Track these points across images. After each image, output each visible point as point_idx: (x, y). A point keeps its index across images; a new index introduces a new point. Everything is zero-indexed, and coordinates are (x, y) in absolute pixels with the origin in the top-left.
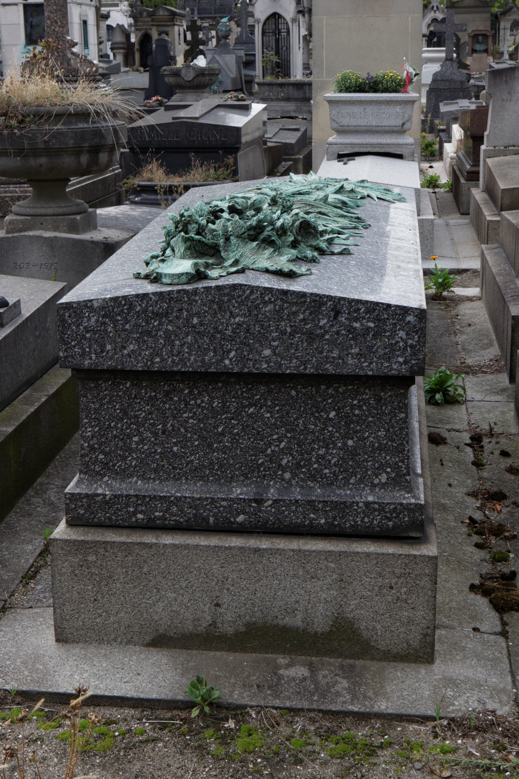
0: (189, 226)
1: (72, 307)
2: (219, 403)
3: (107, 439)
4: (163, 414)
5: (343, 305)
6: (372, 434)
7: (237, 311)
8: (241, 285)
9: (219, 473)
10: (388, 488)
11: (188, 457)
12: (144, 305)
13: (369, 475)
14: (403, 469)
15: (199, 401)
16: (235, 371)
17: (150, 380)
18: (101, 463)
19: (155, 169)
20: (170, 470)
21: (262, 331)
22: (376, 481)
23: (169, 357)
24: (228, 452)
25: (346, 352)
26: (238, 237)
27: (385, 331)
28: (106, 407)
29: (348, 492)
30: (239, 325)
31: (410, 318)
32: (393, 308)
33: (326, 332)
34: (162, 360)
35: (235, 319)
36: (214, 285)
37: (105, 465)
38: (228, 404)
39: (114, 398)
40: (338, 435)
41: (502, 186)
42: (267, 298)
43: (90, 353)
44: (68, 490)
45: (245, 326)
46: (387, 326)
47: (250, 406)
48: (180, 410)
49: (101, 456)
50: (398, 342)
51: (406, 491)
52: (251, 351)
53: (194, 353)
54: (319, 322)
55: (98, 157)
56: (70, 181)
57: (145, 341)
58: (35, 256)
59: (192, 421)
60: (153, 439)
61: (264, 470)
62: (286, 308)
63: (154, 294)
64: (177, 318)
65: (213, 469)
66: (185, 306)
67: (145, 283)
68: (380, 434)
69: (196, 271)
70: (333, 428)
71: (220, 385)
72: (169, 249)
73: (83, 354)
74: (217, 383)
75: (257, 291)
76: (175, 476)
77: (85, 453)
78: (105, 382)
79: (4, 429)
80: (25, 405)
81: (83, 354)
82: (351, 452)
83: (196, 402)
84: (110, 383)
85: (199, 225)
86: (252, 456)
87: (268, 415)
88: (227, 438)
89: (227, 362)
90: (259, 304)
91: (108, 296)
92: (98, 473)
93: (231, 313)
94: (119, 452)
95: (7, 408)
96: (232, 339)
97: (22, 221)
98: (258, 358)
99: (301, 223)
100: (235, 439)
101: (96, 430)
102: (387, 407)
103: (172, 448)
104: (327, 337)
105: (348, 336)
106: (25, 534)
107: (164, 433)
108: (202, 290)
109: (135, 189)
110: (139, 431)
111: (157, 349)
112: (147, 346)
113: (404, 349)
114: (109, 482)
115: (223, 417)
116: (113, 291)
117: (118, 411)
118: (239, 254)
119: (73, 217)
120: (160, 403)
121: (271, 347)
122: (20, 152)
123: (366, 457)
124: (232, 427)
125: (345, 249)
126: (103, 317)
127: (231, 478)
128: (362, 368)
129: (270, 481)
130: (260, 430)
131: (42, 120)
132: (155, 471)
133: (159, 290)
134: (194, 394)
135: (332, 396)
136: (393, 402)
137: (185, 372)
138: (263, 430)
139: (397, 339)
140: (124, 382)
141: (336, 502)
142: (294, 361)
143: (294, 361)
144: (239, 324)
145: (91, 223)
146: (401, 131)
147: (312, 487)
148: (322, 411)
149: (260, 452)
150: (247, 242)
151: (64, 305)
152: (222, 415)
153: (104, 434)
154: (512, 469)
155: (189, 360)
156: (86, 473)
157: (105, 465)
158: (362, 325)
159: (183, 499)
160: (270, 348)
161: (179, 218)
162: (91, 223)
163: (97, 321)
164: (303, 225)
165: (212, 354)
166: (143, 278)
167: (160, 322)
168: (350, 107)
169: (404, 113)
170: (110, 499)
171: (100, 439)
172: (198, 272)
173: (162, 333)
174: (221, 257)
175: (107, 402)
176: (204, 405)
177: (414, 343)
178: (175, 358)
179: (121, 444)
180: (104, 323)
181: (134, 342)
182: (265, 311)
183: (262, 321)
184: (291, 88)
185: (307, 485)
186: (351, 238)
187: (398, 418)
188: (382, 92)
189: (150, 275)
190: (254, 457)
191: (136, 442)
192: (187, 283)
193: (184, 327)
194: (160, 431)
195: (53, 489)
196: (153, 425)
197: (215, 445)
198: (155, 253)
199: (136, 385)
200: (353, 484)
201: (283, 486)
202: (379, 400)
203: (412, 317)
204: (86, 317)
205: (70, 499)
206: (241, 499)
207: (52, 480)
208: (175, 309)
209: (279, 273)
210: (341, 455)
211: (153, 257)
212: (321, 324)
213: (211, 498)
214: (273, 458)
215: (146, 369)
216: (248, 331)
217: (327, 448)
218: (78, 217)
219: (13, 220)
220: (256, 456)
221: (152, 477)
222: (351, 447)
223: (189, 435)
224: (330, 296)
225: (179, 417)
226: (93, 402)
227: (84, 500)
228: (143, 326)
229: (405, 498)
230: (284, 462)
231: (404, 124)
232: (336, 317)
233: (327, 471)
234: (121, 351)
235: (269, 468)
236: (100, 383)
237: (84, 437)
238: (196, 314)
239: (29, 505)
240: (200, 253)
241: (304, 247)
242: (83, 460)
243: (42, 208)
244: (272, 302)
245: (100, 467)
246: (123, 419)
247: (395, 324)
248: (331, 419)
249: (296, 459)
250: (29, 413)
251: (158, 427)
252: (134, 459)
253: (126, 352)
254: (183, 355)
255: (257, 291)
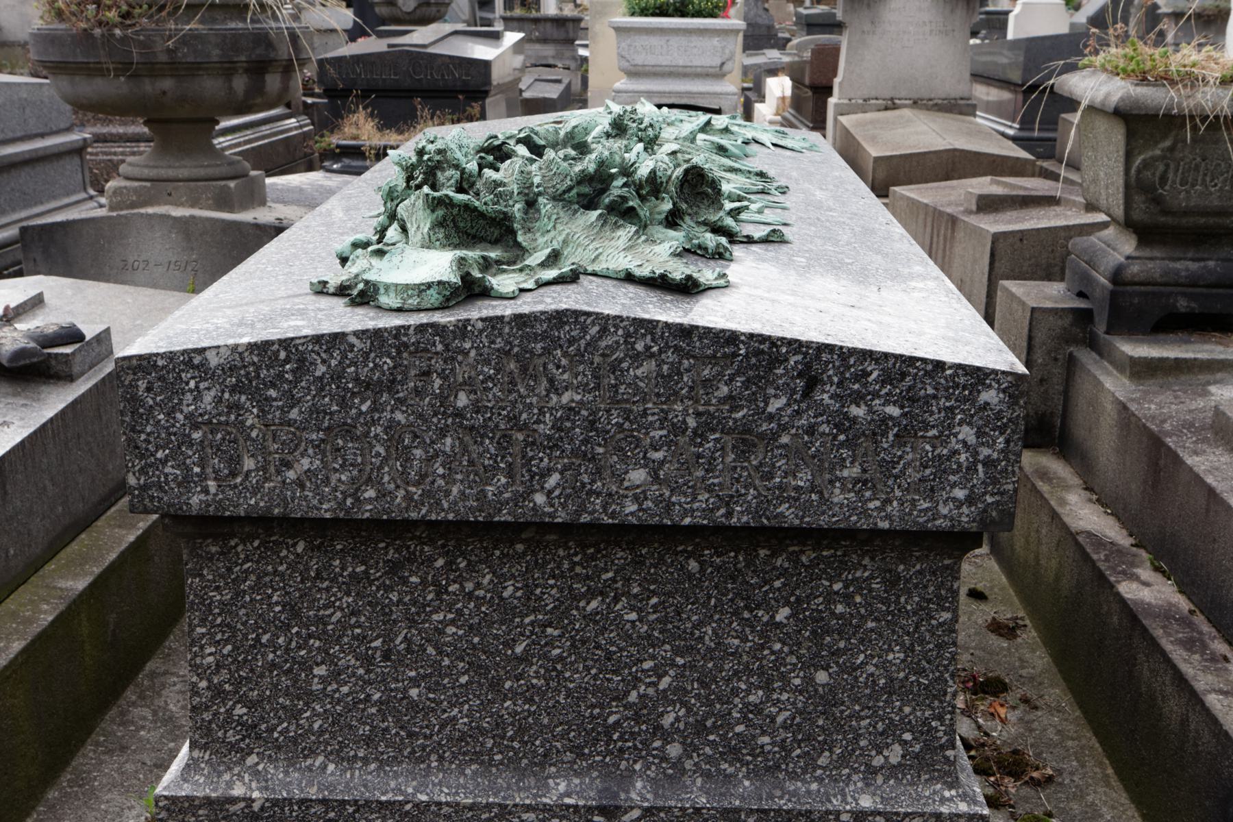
0: (439, 174)
1: (155, 365)
2: (517, 589)
3: (252, 670)
4: (385, 614)
5: (827, 362)
6: (872, 657)
7: (566, 376)
8: (577, 314)
9: (516, 745)
10: (904, 775)
11: (445, 711)
12: (333, 363)
13: (861, 749)
14: (941, 734)
15: (469, 586)
16: (560, 520)
17: (353, 538)
18: (239, 724)
19: (362, 121)
20: (402, 739)
21: (627, 425)
22: (878, 761)
23: (398, 487)
24: (537, 699)
25: (828, 476)
26: (557, 198)
27: (927, 426)
28: (247, 598)
29: (814, 786)
30: (570, 410)
31: (989, 396)
32: (949, 372)
33: (784, 428)
34: (382, 494)
35: (560, 395)
36: (508, 312)
37: (250, 729)
38: (538, 591)
39: (267, 579)
40: (794, 660)
41: (874, 152)
42: (640, 346)
43: (203, 477)
44: (159, 790)
45: (584, 413)
46: (932, 413)
47: (591, 595)
48: (424, 606)
49: (240, 710)
50: (955, 452)
51: (945, 783)
52: (598, 473)
53: (459, 477)
54: (767, 404)
55: (264, 81)
56: (217, 123)
57: (339, 450)
58: (158, 248)
59: (454, 630)
60: (361, 671)
61: (621, 738)
62: (688, 371)
63: (359, 334)
64: (417, 392)
65: (503, 738)
66: (438, 364)
67: (339, 303)
68: (890, 657)
69: (462, 278)
70: (784, 644)
71: (520, 547)
72: (395, 225)
73: (186, 481)
74: (512, 544)
75: (616, 327)
76: (413, 752)
77: (201, 703)
78: (243, 541)
79: (70, 583)
80: (120, 527)
81: (186, 481)
82: (822, 697)
83: (463, 588)
84: (256, 543)
85: (463, 171)
86: (593, 706)
87: (633, 616)
88: (534, 668)
89: (540, 499)
90: (621, 361)
91: (245, 340)
92: (233, 747)
93: (551, 381)
94: (281, 700)
95: (83, 536)
96: (553, 445)
97: (135, 190)
98: (614, 488)
99: (687, 171)
100: (555, 669)
101: (225, 651)
102: (910, 597)
103: (405, 690)
104: (785, 439)
105: (835, 437)
106: (109, 796)
107: (386, 656)
108: (480, 325)
109: (332, 151)
110: (327, 654)
111: (368, 468)
112: (345, 460)
113: (968, 469)
114: (260, 767)
115: (527, 620)
116: (259, 325)
117: (278, 609)
118: (561, 239)
119: (223, 183)
120: (378, 589)
121: (646, 463)
122: (124, 67)
123: (857, 708)
124: (546, 644)
125: (774, 231)
126: (232, 392)
127: (545, 756)
128: (865, 513)
129: (635, 762)
130: (614, 649)
131: (164, 14)
132: (368, 741)
133: (370, 325)
134: (458, 569)
135: (784, 573)
136: (926, 587)
137: (436, 521)
138: (621, 650)
139: (954, 444)
140: (291, 542)
141: (788, 812)
142: (704, 496)
143: (704, 496)
144: (571, 409)
145: (256, 197)
146: (718, 74)
147: (731, 775)
148: (758, 607)
149: (613, 699)
150: (576, 212)
151: (134, 362)
152: (523, 616)
153: (245, 660)
154: (1000, 627)
155: (448, 493)
156: (205, 747)
157: (250, 729)
158: (871, 411)
159: (433, 808)
160: (645, 466)
161: (414, 159)
162: (256, 197)
163: (218, 400)
164: (689, 177)
165: (503, 480)
166: (334, 294)
167: (374, 402)
168: (645, 37)
169: (723, 48)
170: (262, 808)
171: (237, 671)
172: (466, 278)
173: (379, 429)
174: (518, 245)
175: (250, 587)
176: (481, 593)
177: (995, 455)
178: (413, 489)
179: (285, 682)
180: (235, 407)
181: (310, 451)
182: (636, 377)
183: (627, 401)
184: (549, 25)
185: (719, 771)
186: (766, 211)
187: (934, 622)
188: (693, 16)
189: (349, 287)
190: (597, 711)
191: (321, 677)
192: (443, 307)
193: (435, 415)
194: (379, 653)
195: (175, 685)
196: (362, 639)
197: (508, 684)
198: (361, 237)
199: (319, 547)
200: (823, 768)
201: (664, 772)
202: (892, 581)
203: (993, 393)
204: (191, 391)
205: (168, 810)
206: (568, 806)
207: (174, 665)
208: (413, 373)
209: (660, 284)
210: (800, 705)
211: (355, 245)
212: (771, 409)
213: (500, 805)
214: (644, 712)
215: (341, 515)
216: (592, 424)
217: (768, 688)
218: (232, 184)
219: (121, 188)
220: (602, 707)
221: (361, 754)
222: (823, 686)
223: (446, 662)
224: (796, 341)
225: (423, 622)
226: (217, 588)
227: (201, 812)
228: (331, 414)
229: (943, 800)
230: (667, 720)
231: (723, 64)
232: (808, 392)
233: (766, 739)
234: (279, 472)
235: (632, 733)
236: (233, 543)
237: (197, 666)
238: (464, 383)
239: (123, 724)
240: (468, 235)
241: (693, 224)
242: (198, 718)
243: (170, 167)
244: (652, 355)
245: (238, 733)
246: (289, 627)
247: (951, 409)
248: (779, 625)
249: (696, 714)
250: (124, 546)
251: (373, 645)
252: (318, 715)
253: (291, 475)
254: (433, 482)
255: (616, 327)
